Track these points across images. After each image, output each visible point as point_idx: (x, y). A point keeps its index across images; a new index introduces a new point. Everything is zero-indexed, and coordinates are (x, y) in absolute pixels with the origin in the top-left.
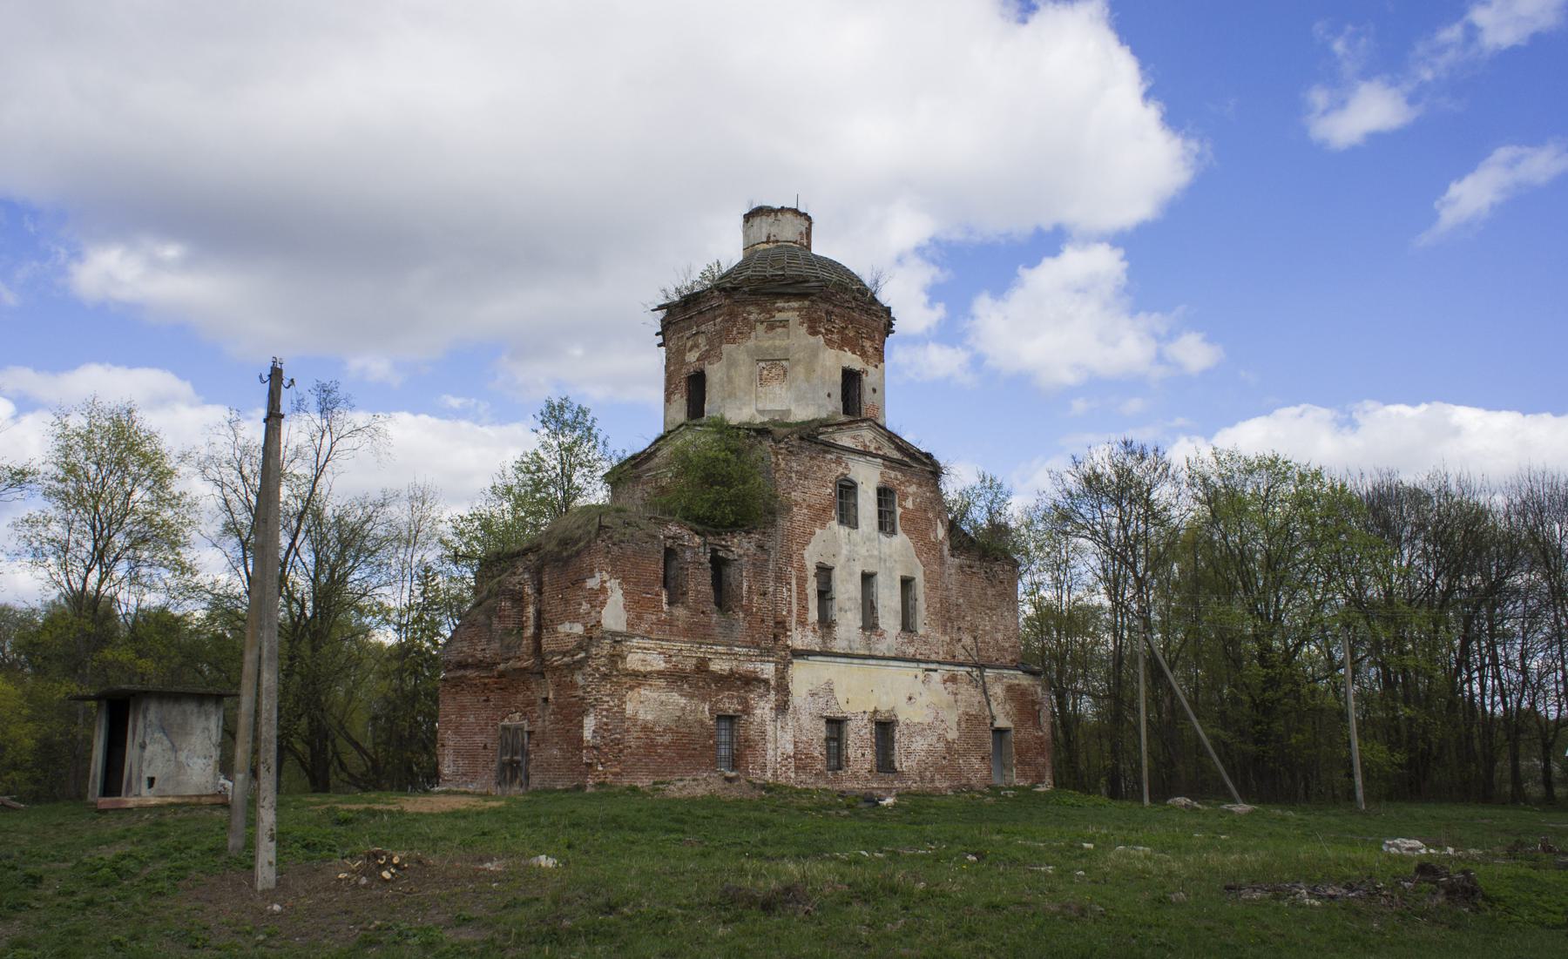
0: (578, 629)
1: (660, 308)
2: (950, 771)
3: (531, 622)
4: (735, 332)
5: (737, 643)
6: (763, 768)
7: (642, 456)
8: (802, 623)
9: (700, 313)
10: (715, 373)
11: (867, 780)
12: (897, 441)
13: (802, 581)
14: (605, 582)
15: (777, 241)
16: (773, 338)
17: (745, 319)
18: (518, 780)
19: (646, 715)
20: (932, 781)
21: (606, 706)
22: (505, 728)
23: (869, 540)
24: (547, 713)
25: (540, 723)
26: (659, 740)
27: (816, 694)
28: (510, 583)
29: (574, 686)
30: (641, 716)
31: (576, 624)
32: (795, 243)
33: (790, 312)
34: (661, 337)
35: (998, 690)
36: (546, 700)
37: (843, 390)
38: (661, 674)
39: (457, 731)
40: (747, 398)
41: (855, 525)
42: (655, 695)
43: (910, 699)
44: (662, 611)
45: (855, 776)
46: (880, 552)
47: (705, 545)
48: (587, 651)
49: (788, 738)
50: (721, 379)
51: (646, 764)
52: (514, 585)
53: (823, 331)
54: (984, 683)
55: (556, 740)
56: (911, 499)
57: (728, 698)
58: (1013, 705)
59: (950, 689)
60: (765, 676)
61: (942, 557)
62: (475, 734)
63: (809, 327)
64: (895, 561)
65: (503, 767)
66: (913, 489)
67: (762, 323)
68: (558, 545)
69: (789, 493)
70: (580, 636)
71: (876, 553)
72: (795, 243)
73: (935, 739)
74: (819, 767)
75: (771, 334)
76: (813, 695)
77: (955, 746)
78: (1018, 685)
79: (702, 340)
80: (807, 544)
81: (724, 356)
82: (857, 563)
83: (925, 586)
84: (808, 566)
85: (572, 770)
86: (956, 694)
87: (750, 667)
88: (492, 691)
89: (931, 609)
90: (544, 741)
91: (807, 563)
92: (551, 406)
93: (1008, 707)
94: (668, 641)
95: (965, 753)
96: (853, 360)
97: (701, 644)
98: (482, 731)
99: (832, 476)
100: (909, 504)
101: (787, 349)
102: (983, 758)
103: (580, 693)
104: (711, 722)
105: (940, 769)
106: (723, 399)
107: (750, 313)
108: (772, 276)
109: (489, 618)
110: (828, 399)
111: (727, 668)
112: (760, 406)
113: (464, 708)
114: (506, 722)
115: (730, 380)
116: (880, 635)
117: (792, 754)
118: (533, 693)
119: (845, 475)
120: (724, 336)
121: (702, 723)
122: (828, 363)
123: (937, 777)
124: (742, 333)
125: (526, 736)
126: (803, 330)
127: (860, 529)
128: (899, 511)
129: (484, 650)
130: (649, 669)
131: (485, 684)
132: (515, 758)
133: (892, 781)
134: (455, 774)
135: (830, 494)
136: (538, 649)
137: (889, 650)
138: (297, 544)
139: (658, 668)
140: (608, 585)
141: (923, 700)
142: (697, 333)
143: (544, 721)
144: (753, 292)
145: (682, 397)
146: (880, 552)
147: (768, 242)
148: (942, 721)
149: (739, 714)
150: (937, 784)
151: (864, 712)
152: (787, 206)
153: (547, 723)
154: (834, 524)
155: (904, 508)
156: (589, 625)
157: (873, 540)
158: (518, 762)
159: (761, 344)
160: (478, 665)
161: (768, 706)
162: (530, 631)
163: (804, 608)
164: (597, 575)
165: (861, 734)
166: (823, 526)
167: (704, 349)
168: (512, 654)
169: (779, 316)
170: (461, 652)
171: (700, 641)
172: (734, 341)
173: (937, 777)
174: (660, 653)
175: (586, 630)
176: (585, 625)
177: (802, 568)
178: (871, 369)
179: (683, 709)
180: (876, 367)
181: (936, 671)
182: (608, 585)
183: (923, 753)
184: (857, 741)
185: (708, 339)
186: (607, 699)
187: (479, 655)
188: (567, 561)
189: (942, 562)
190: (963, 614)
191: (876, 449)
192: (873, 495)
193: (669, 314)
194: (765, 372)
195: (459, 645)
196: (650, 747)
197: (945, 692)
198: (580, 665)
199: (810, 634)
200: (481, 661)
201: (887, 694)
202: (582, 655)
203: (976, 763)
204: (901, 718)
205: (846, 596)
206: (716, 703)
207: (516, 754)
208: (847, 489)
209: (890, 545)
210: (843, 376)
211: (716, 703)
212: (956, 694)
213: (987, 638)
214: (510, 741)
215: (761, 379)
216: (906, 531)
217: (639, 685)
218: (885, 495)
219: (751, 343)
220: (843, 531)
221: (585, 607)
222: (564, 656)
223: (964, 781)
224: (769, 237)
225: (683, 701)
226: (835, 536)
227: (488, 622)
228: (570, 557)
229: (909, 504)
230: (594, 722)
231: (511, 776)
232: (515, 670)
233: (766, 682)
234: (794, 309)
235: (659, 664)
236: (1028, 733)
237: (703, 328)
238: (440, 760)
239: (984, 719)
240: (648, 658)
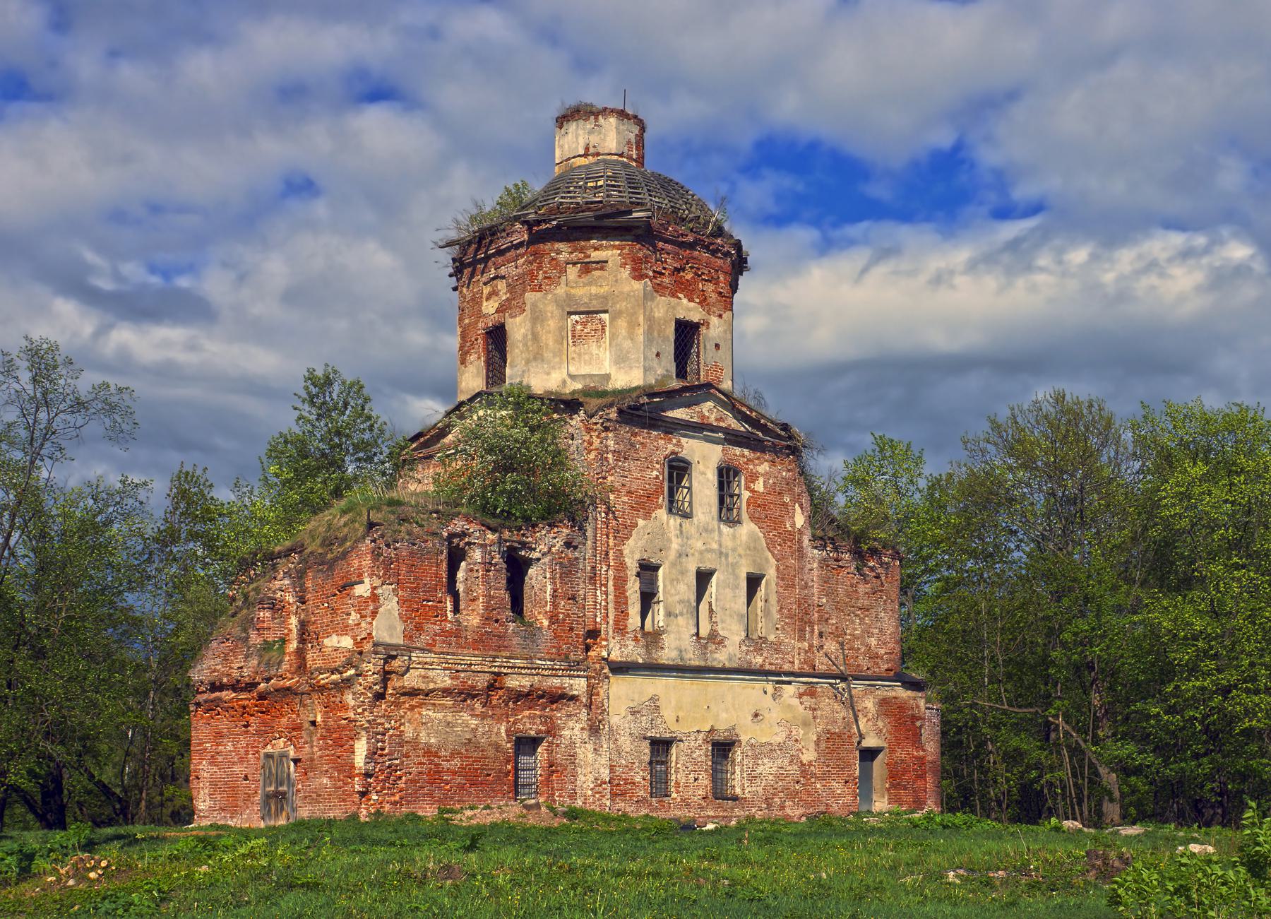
0: (347, 642)
1: (449, 244)
2: (805, 797)
3: (294, 634)
4: (540, 277)
5: (539, 655)
6: (573, 795)
7: (433, 433)
8: (621, 629)
9: (500, 252)
10: (517, 328)
11: (702, 808)
12: (744, 409)
13: (620, 583)
14: (375, 588)
15: (598, 154)
16: (590, 284)
17: (553, 259)
18: (284, 813)
19: (428, 738)
20: (782, 808)
21: (380, 729)
22: (268, 756)
23: (706, 530)
24: (315, 738)
25: (307, 748)
26: (446, 765)
27: (639, 712)
28: (270, 589)
29: (345, 707)
30: (423, 738)
31: (344, 637)
32: (621, 155)
33: (609, 252)
34: (454, 278)
35: (869, 704)
36: (313, 723)
37: (676, 348)
38: (446, 692)
39: (213, 761)
40: (557, 359)
41: (687, 516)
42: (440, 715)
43: (756, 715)
44: (446, 620)
45: (686, 803)
46: (720, 545)
47: (500, 543)
48: (356, 667)
49: (603, 762)
50: (525, 336)
51: (430, 794)
52: (274, 592)
53: (651, 274)
54: (851, 697)
55: (325, 768)
56: (761, 480)
57: (529, 717)
58: (887, 721)
59: (807, 704)
60: (575, 693)
61: (800, 550)
62: (234, 763)
63: (634, 269)
64: (740, 555)
65: (268, 797)
66: (764, 467)
67: (574, 264)
68: (322, 545)
69: (605, 478)
70: (349, 651)
71: (715, 546)
72: (621, 155)
73: (787, 761)
74: (641, 793)
75: (586, 279)
76: (633, 713)
77: (812, 768)
78: (895, 698)
79: (501, 285)
80: (628, 538)
81: (528, 308)
82: (690, 558)
83: (777, 585)
84: (629, 564)
85: (344, 800)
86: (815, 709)
87: (556, 682)
88: (252, 715)
89: (786, 611)
90: (312, 769)
91: (626, 560)
92: (311, 378)
93: (880, 724)
94: (453, 654)
95: (824, 777)
96: (689, 310)
97: (494, 657)
98: (241, 760)
99: (660, 455)
100: (759, 486)
101: (605, 298)
102: (846, 782)
103: (351, 715)
104: (509, 745)
105: (793, 795)
106: (528, 362)
107: (559, 252)
108: (587, 203)
109: (245, 630)
110: (656, 360)
111: (528, 684)
112: (573, 370)
113: (219, 735)
114: (269, 749)
115: (535, 337)
116: (719, 644)
117: (607, 780)
118: (298, 715)
119: (676, 453)
120: (527, 282)
121: (497, 747)
122: (656, 315)
123: (788, 803)
124: (549, 278)
125: (292, 764)
126: (625, 273)
127: (695, 519)
128: (746, 495)
129: (241, 668)
130: (431, 686)
131: (244, 707)
132: (280, 789)
133: (732, 809)
134: (212, 809)
135: (657, 477)
136: (301, 667)
137: (730, 659)
138: (12, 543)
139: (442, 685)
140: (379, 591)
141: (774, 713)
142: (496, 278)
143: (312, 747)
144: (541, 235)
145: (479, 358)
146: (720, 545)
147: (585, 155)
148: (796, 740)
149: (543, 735)
150: (788, 811)
151: (698, 731)
152: (611, 106)
153: (316, 749)
154: (662, 514)
155: (753, 491)
156: (359, 638)
157: (712, 531)
158: (284, 794)
159: (573, 291)
160: (235, 687)
161: (579, 726)
162: (293, 646)
163: (623, 614)
164: (367, 580)
165: (695, 756)
166: (647, 516)
167: (504, 298)
168: (272, 673)
169: (596, 255)
170: (214, 671)
171: (494, 653)
172: (539, 288)
173: (788, 803)
174: (445, 669)
175: (356, 644)
176: (354, 638)
177: (621, 566)
178: (714, 320)
179: (474, 730)
180: (720, 316)
181: (789, 683)
182: (379, 591)
183: (771, 777)
184: (688, 765)
185: (508, 285)
186: (382, 720)
187: (236, 674)
188: (332, 565)
189: (801, 555)
190: (827, 616)
191: (716, 420)
192: (712, 477)
193: (464, 251)
194: (579, 327)
195: (212, 662)
196: (435, 775)
197: (801, 708)
198: (348, 683)
199: (631, 643)
200: (238, 681)
201: (727, 710)
202: (352, 672)
203: (838, 787)
204: (744, 738)
205: (677, 598)
206: (515, 723)
207: (281, 785)
208: (678, 470)
209: (734, 537)
210: (676, 330)
211: (515, 723)
212: (815, 709)
213: (857, 644)
214: (274, 771)
215: (574, 336)
216: (752, 518)
217: (420, 705)
218: (726, 475)
219: (561, 291)
220: (674, 522)
221: (354, 616)
222: (333, 673)
223: (822, 808)
224: (587, 149)
225: (474, 722)
226: (662, 532)
227: (244, 635)
228: (335, 560)
229: (759, 486)
230: (365, 747)
231: (277, 809)
232: (277, 690)
233: (574, 698)
234: (614, 247)
235: (444, 680)
236: (905, 753)
237: (503, 271)
238: (194, 793)
239: (850, 737)
240: (431, 674)
